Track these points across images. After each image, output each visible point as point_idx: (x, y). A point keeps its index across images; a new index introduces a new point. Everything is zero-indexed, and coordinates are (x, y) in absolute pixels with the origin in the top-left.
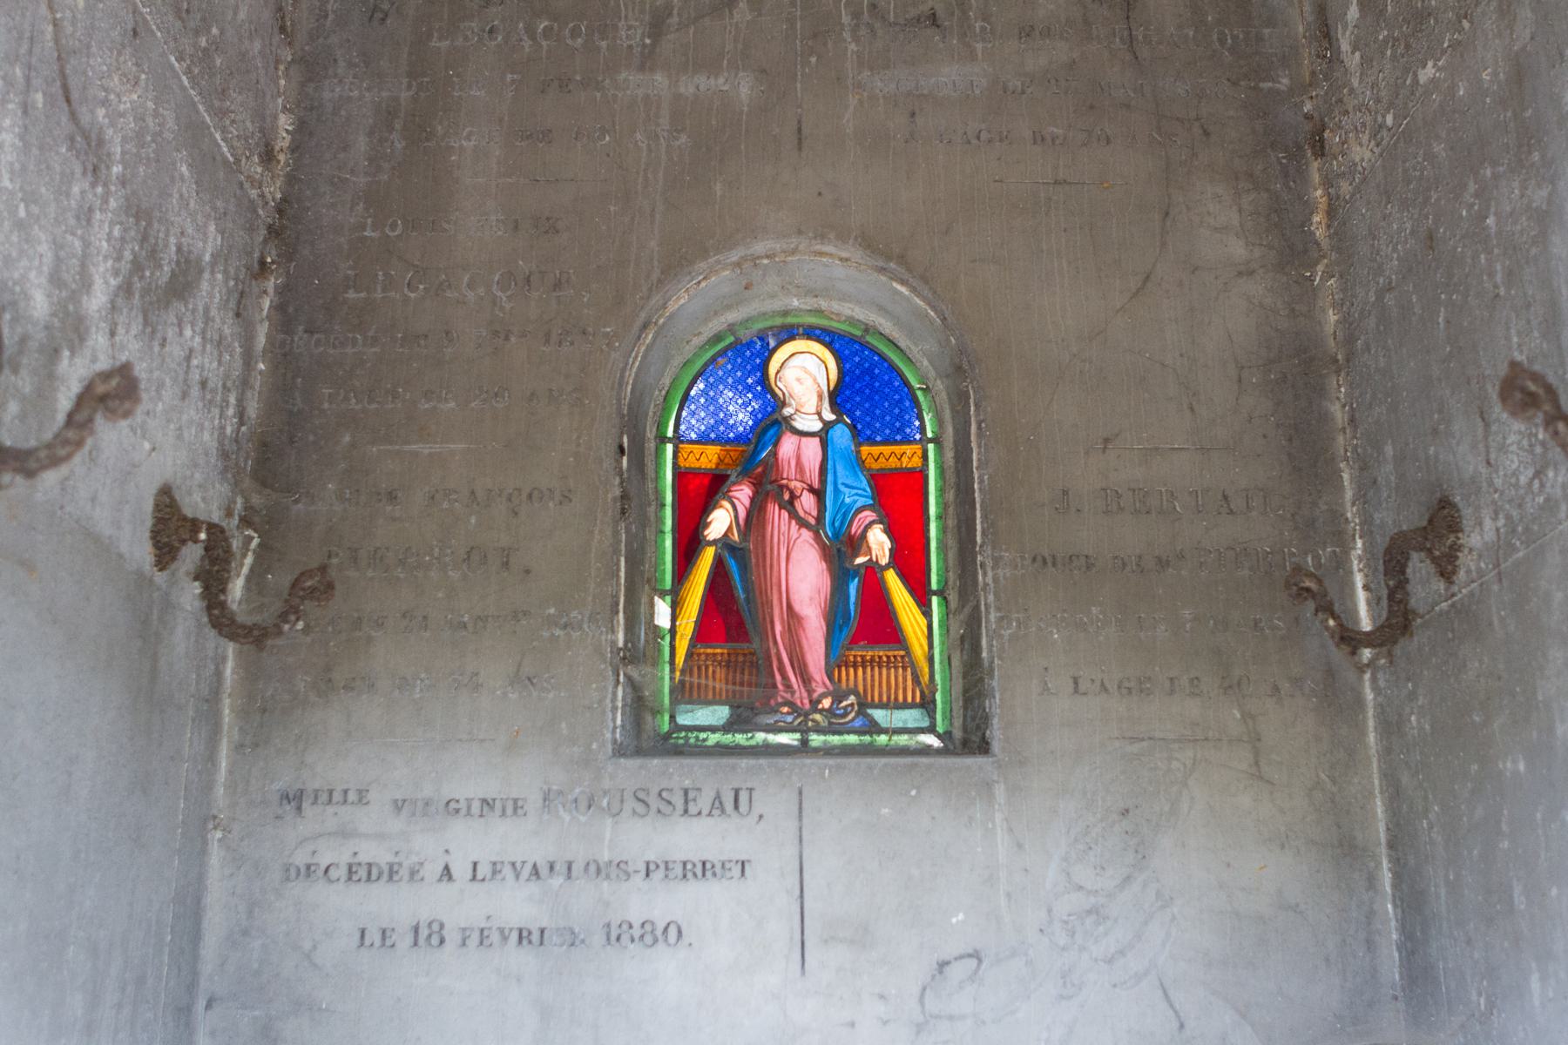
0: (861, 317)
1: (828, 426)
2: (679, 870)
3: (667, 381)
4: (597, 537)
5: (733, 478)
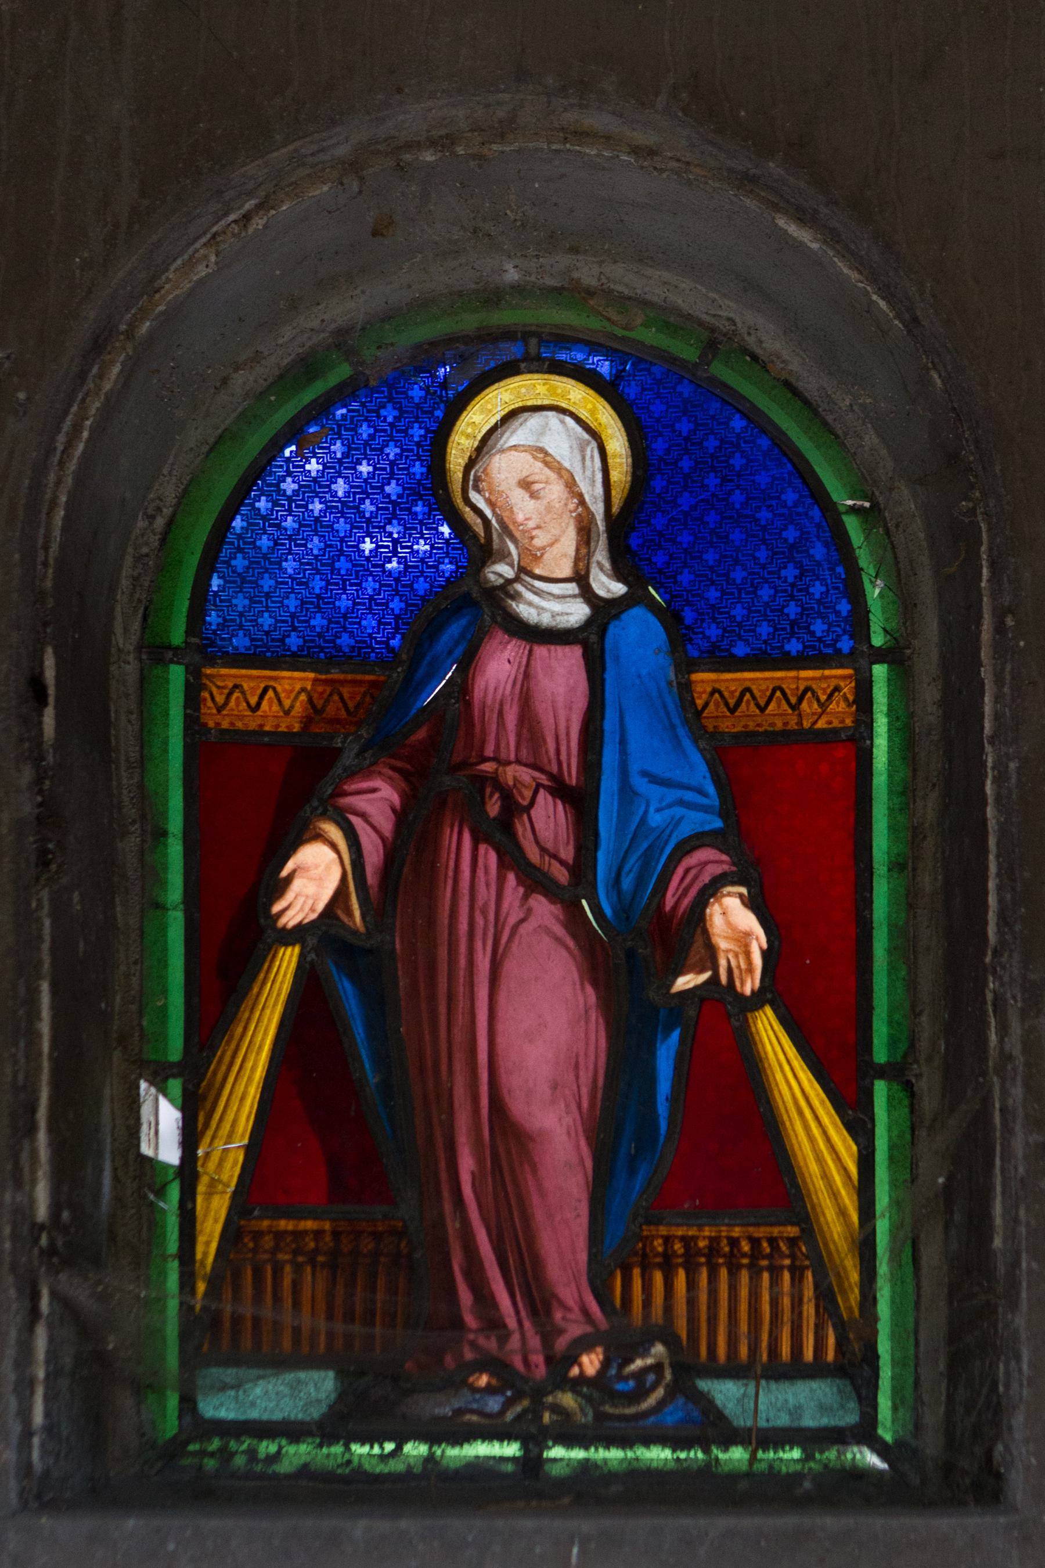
0: (700, 309)
1: (604, 611)
3: (170, 493)
5: (348, 759)
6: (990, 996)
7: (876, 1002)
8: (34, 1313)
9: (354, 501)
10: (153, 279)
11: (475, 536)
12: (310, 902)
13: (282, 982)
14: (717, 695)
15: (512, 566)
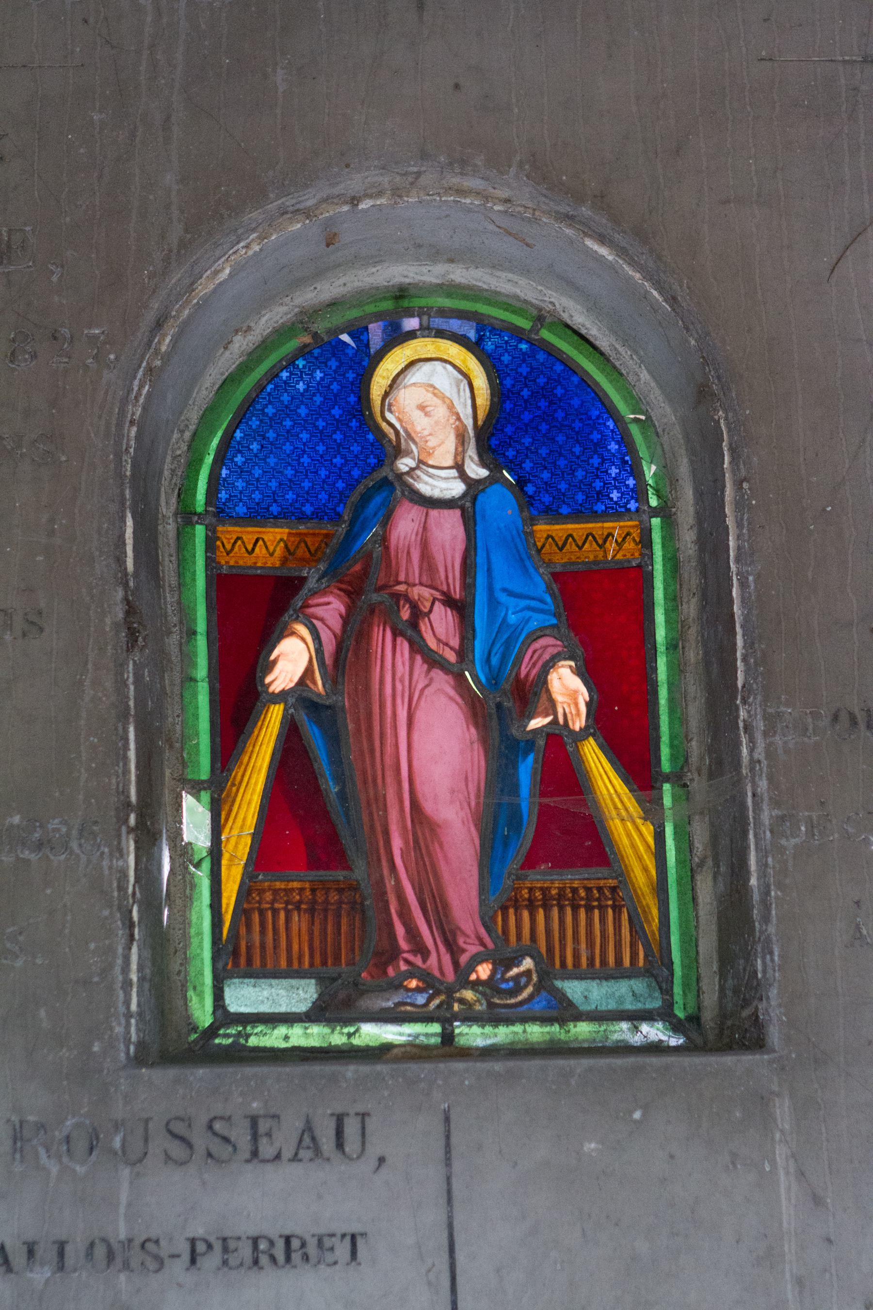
1: (474, 487)
2: (246, 1251)
5: (311, 583)
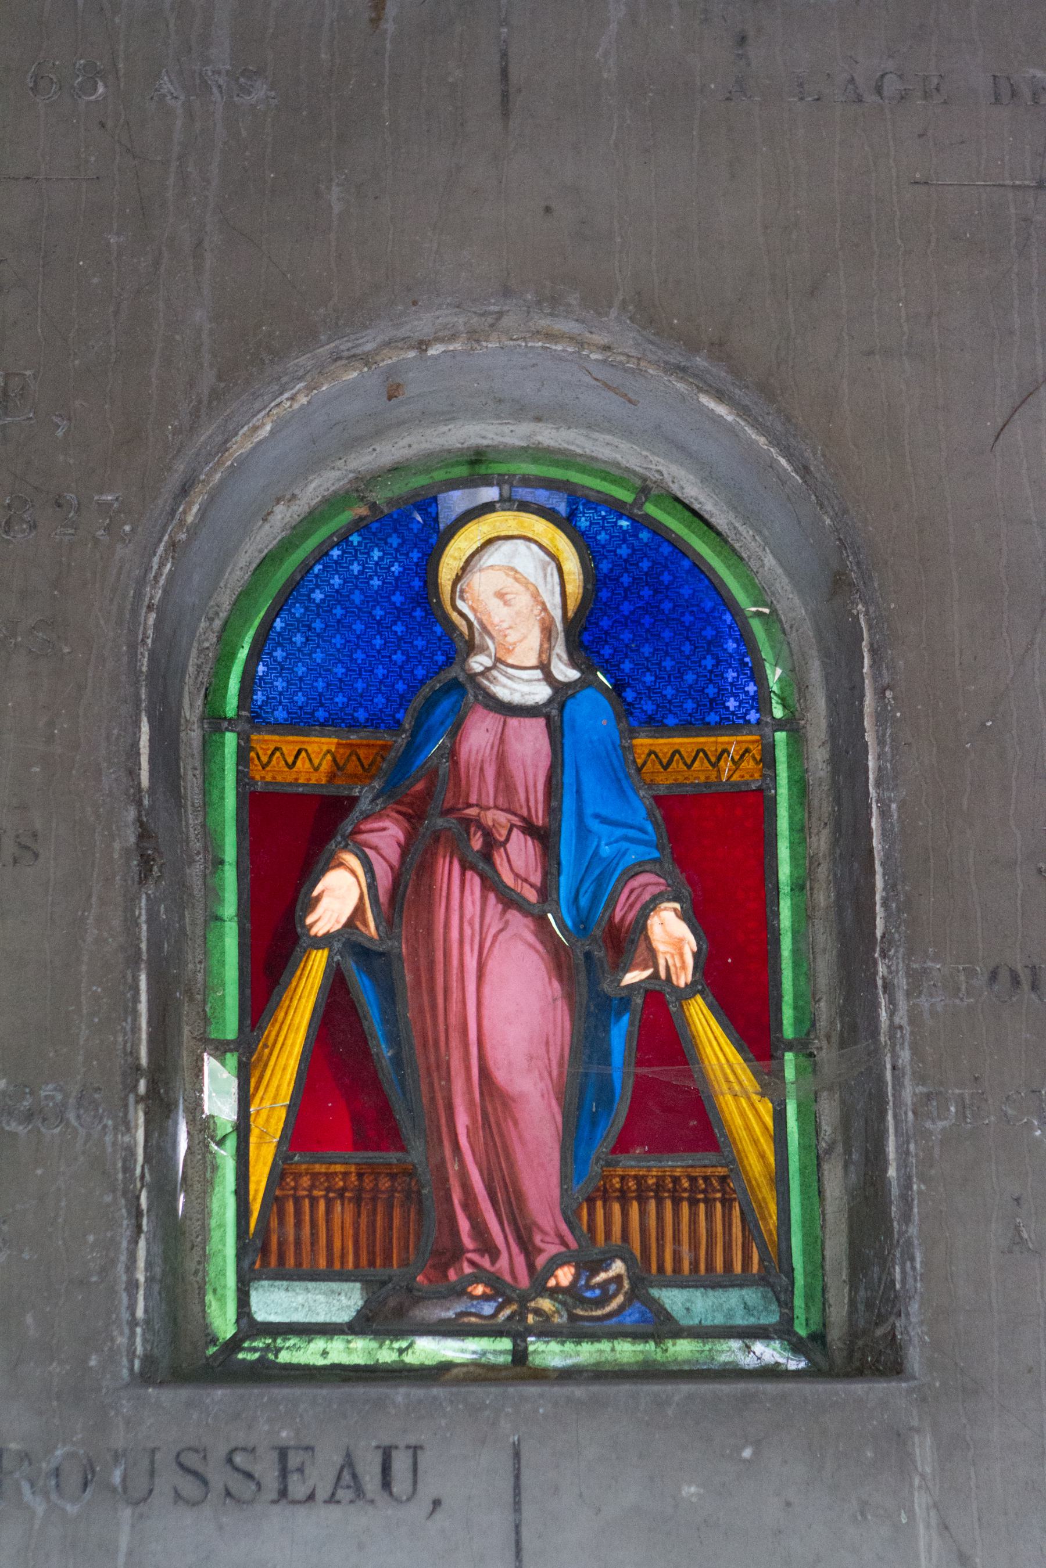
4: (92, 933)
5: (364, 805)
6: (880, 982)
7: (784, 993)
8: (139, 1227)
9: (368, 607)
10: (226, 442)
11: (461, 634)
12: (335, 915)
13: (315, 978)
14: (653, 756)
15: (489, 656)
